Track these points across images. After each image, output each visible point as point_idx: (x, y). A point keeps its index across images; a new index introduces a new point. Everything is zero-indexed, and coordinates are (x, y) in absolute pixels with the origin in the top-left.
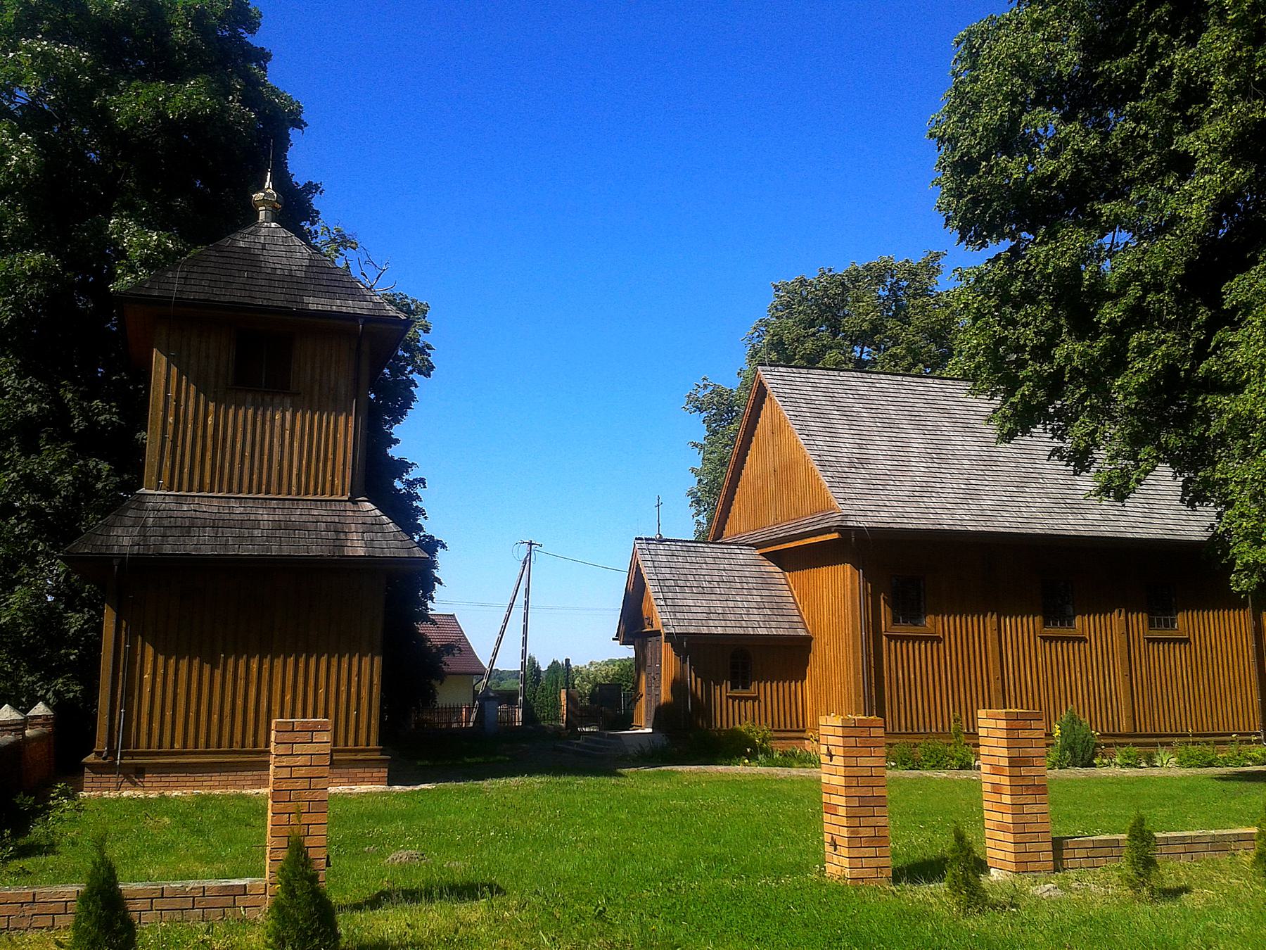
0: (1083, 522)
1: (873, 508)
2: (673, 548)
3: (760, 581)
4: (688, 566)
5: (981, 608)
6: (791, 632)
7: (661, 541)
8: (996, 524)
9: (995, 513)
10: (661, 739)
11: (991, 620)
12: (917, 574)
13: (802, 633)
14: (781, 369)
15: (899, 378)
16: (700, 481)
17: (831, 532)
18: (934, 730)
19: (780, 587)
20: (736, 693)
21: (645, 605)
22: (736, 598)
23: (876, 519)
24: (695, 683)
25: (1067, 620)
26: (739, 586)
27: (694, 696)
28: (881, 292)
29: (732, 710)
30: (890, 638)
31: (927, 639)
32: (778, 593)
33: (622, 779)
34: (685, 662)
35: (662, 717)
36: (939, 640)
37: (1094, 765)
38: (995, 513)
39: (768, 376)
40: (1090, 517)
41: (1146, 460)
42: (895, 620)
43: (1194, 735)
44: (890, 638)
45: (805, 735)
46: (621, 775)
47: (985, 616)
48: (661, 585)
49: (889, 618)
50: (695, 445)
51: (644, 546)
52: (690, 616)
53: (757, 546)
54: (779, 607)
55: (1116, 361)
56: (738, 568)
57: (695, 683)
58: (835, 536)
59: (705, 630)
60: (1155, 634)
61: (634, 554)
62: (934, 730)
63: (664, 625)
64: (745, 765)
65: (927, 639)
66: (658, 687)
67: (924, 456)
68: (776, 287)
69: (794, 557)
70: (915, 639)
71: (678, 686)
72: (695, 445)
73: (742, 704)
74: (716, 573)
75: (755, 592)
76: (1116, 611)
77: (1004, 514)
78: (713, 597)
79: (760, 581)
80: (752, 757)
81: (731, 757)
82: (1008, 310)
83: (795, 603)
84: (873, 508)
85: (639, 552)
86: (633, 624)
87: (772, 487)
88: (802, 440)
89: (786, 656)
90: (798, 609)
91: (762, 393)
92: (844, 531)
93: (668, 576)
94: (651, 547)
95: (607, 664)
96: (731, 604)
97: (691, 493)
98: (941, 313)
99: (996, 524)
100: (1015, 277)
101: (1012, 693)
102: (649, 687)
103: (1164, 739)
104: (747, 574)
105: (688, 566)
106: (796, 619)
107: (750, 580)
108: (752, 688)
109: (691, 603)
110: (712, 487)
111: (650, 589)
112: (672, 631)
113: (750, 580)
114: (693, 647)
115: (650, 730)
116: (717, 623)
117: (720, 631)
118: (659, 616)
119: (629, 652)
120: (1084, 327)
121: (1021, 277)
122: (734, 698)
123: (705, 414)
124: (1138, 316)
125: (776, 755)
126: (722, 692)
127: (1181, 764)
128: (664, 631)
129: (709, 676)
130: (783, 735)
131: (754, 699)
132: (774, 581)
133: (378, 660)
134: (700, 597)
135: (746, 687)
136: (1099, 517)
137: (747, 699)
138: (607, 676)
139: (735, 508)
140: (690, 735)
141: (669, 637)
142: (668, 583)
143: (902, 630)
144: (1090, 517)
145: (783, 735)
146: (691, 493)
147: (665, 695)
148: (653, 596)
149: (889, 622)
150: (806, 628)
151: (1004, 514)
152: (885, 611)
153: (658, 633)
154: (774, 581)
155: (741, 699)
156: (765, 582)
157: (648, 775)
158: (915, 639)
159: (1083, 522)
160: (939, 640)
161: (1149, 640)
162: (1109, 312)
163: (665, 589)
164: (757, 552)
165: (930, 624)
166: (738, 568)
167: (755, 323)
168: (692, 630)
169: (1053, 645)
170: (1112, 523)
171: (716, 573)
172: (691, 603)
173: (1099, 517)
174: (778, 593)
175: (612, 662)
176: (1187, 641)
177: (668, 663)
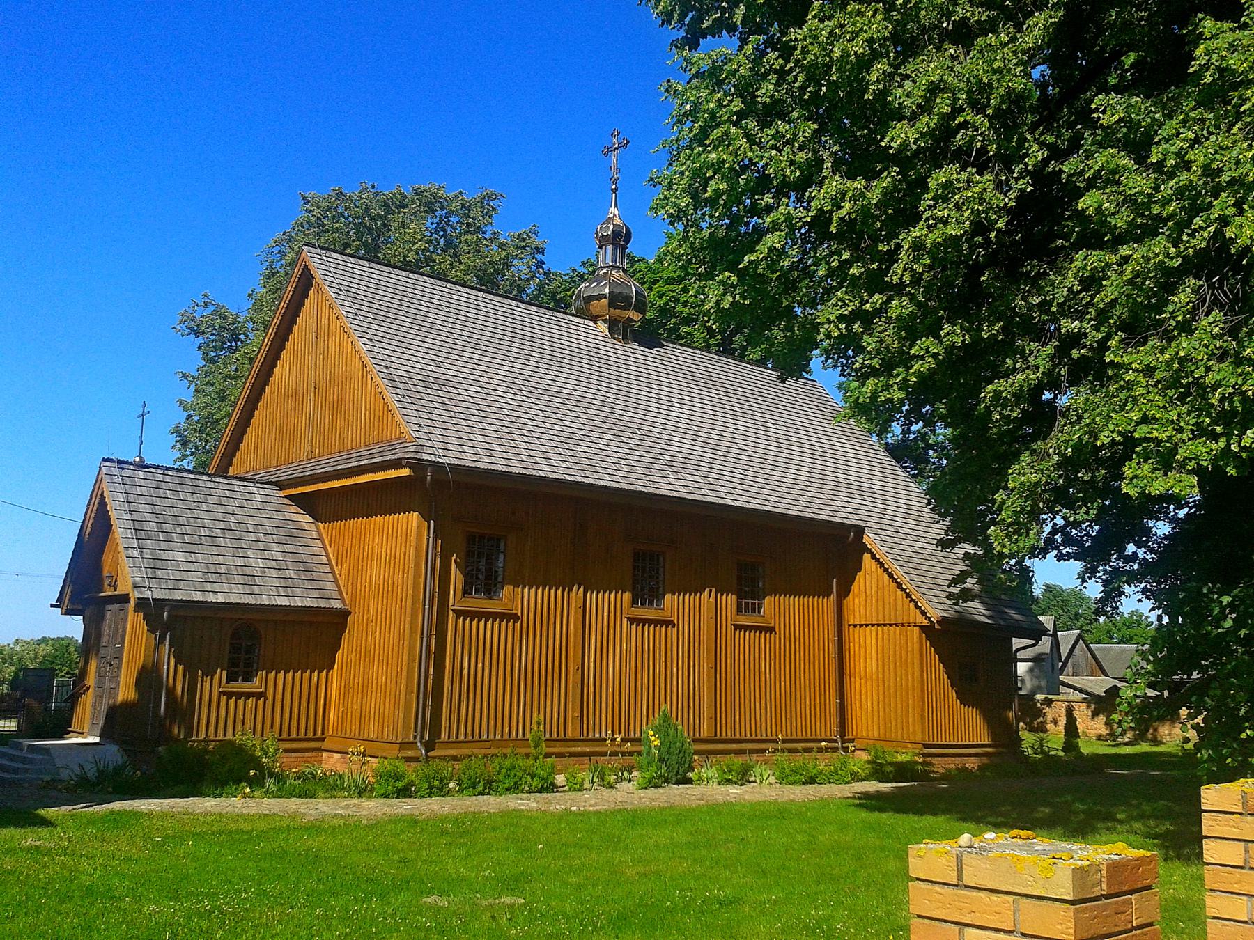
0: (684, 483)
1: (454, 441)
2: (160, 478)
3: (282, 532)
4: (179, 504)
5: (566, 583)
6: (322, 604)
7: (142, 466)
8: (595, 475)
9: (593, 462)
10: (114, 754)
11: (577, 593)
12: (499, 528)
13: (337, 604)
14: (334, 255)
15: (479, 294)
16: (189, 417)
17: (402, 467)
18: (498, 737)
19: (310, 542)
20: (239, 686)
21: (107, 559)
22: (249, 553)
23: (458, 455)
24: (172, 673)
25: (654, 597)
26: (252, 536)
27: (171, 692)
28: (428, 224)
29: (223, 712)
30: (458, 614)
31: (501, 616)
32: (307, 550)
33: (44, 831)
34: (162, 641)
35: (118, 722)
36: (516, 618)
37: (690, 781)
38: (593, 462)
39: (317, 261)
40: (690, 478)
41: (922, 358)
42: (467, 592)
43: (784, 741)
44: (458, 614)
45: (325, 745)
46: (45, 823)
47: (570, 590)
48: (137, 529)
49: (460, 586)
50: (185, 376)
51: (116, 471)
52: (178, 575)
53: (281, 485)
54: (308, 568)
55: (903, 212)
56: (253, 512)
57: (172, 673)
58: (405, 472)
59: (198, 597)
60: (743, 620)
61: (98, 482)
62: (498, 737)
63: (135, 586)
64: (245, 796)
65: (501, 616)
66: (115, 678)
67: (511, 386)
68: (304, 198)
69: (330, 502)
70: (488, 616)
71: (148, 678)
72: (185, 376)
73: (241, 702)
74: (220, 517)
75: (275, 547)
76: (707, 590)
77: (603, 464)
78: (215, 550)
79: (282, 532)
80: (257, 783)
81: (224, 784)
82: (751, 123)
83: (330, 564)
84: (454, 441)
85: (106, 479)
86: (85, 587)
87: (308, 409)
88: (362, 344)
89: (312, 636)
90: (333, 572)
91: (307, 281)
92: (418, 465)
93: (148, 517)
94: (125, 473)
95: (39, 642)
96: (240, 562)
97: (177, 431)
98: (496, 254)
99: (595, 475)
100: (764, 77)
101: (592, 689)
102: (100, 676)
103: (758, 746)
104: (265, 522)
105: (179, 504)
106: (329, 586)
107: (269, 530)
108: (257, 680)
109: (180, 556)
110: (209, 423)
111: (118, 532)
112: (148, 595)
113: (269, 530)
114: (169, 618)
115: (97, 740)
116: (217, 587)
117: (220, 598)
118: (128, 572)
119: (74, 628)
120: (862, 161)
121: (773, 78)
122: (229, 695)
123: (200, 340)
124: (941, 147)
125: (291, 781)
126: (215, 684)
127: (782, 780)
128: (135, 595)
129: (194, 662)
130: (294, 745)
131: (259, 696)
132: (301, 533)
133: (225, 672)
134: (194, 548)
135: (248, 678)
136: (698, 479)
137: (248, 695)
138: (36, 657)
139: (250, 437)
140: (157, 753)
141: (142, 604)
142: (147, 526)
143: (477, 603)
144: (690, 478)
145: (294, 745)
146: (177, 431)
147: (126, 691)
148: (122, 544)
149: (459, 594)
150: (342, 599)
151: (603, 464)
152: (456, 579)
153: (124, 598)
154: (301, 533)
155: (239, 695)
156: (290, 534)
157: (93, 821)
158: (488, 616)
159: (684, 483)
160: (516, 618)
161: (737, 627)
162: (901, 135)
163: (142, 535)
164: (282, 494)
165: (509, 596)
166: (253, 512)
167: (278, 235)
168: (178, 595)
169: (640, 628)
170: (712, 487)
171: (220, 517)
172: (180, 556)
173: (698, 479)
174: (307, 550)
175: (44, 640)
176: (771, 630)
177: (135, 641)
